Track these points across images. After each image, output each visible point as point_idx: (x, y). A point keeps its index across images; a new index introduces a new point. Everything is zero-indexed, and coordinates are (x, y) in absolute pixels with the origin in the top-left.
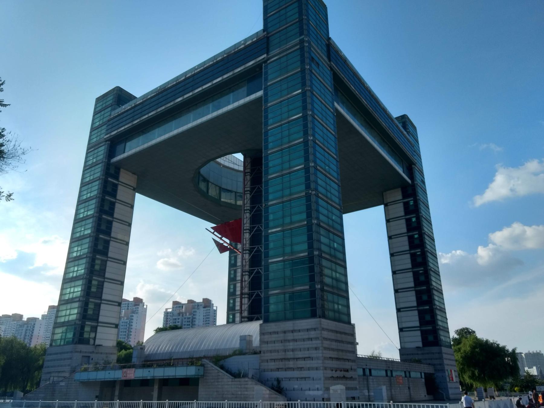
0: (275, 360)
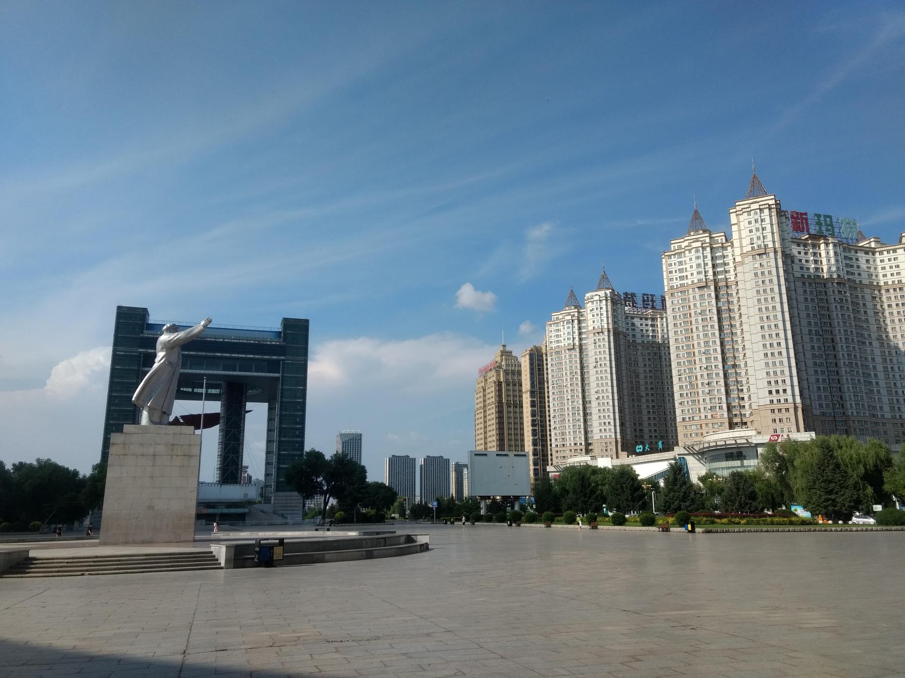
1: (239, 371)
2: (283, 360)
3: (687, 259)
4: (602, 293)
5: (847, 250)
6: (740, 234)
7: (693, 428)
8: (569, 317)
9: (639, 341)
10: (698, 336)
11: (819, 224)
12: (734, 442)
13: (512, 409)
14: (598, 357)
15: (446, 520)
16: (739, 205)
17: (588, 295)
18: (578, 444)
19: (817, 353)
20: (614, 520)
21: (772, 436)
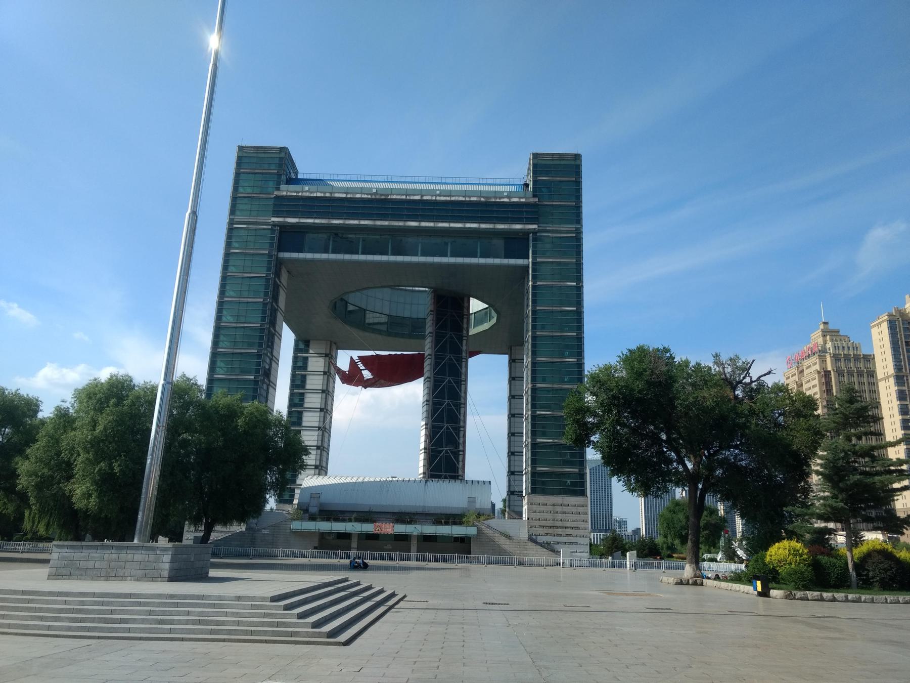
0: (543, 526)
1: (451, 256)
2: (535, 232)
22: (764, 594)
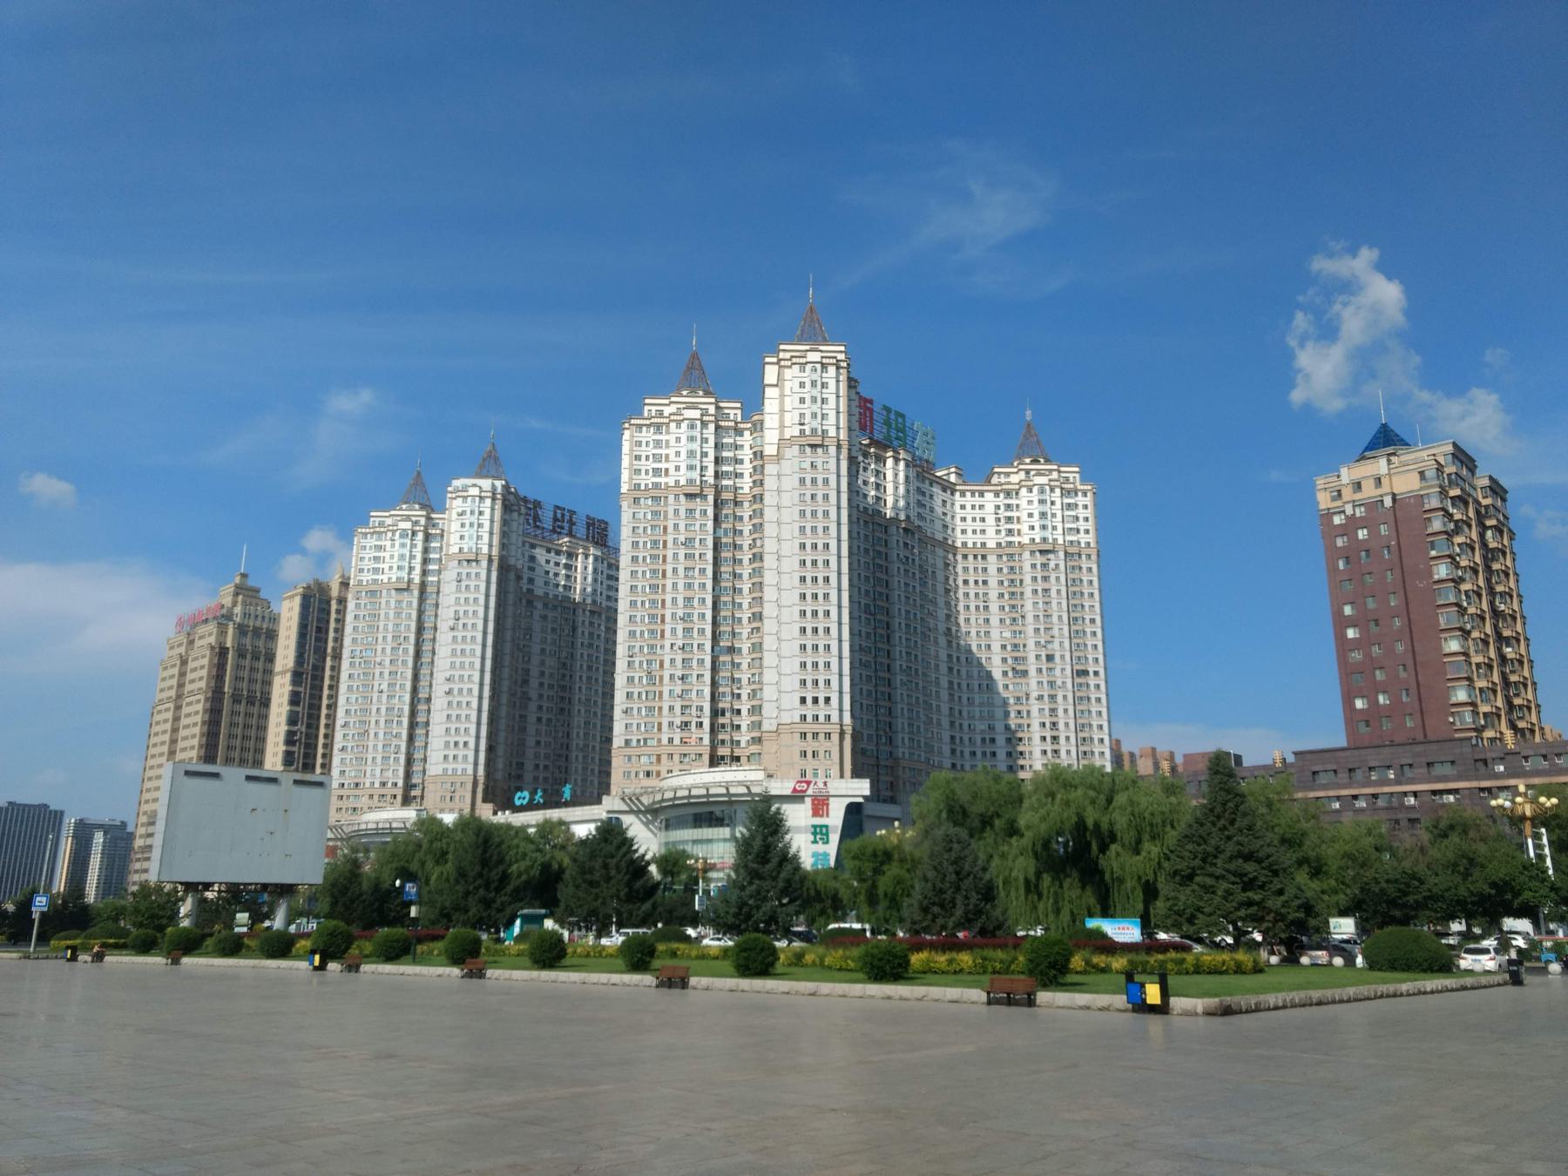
3: (672, 438)
4: (486, 484)
5: (920, 478)
6: (782, 403)
7: (642, 760)
8: (407, 525)
9: (539, 592)
10: (675, 585)
11: (887, 423)
12: (724, 791)
13: (242, 708)
14: (461, 610)
15: (74, 949)
16: (784, 350)
17: (457, 483)
18: (390, 785)
19: (864, 644)
20: (747, 959)
21: (798, 782)
22: (322, 967)
